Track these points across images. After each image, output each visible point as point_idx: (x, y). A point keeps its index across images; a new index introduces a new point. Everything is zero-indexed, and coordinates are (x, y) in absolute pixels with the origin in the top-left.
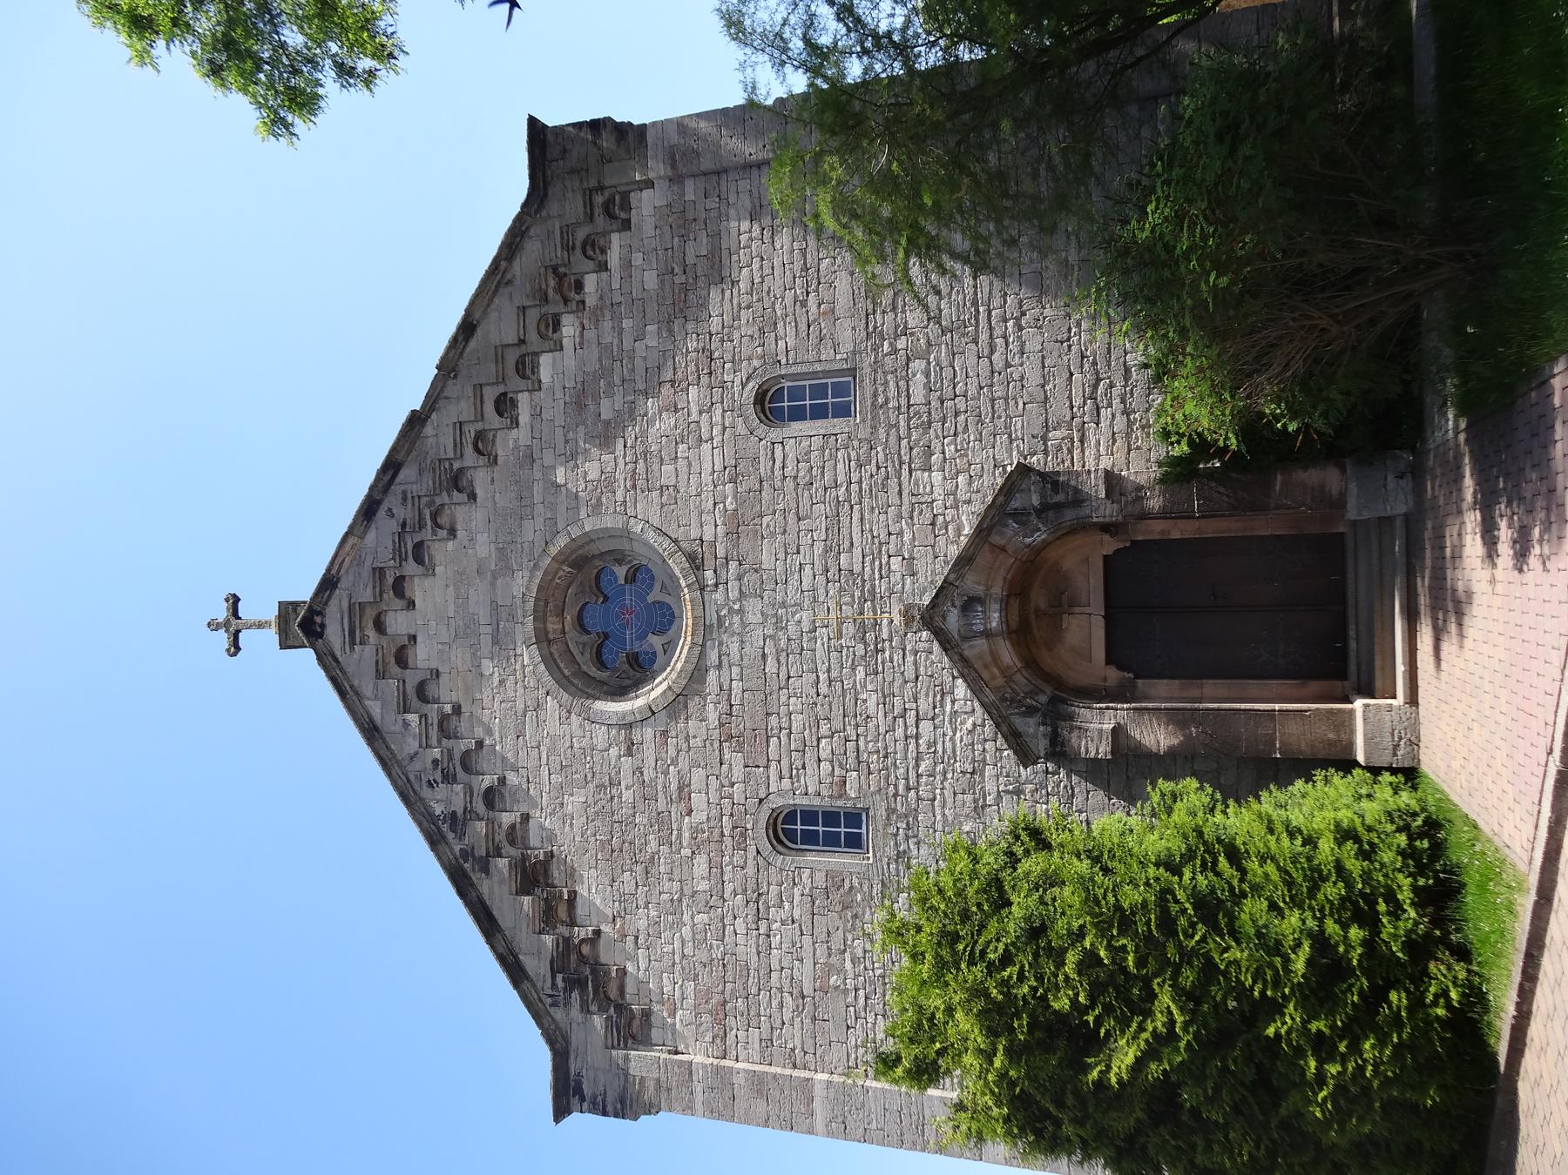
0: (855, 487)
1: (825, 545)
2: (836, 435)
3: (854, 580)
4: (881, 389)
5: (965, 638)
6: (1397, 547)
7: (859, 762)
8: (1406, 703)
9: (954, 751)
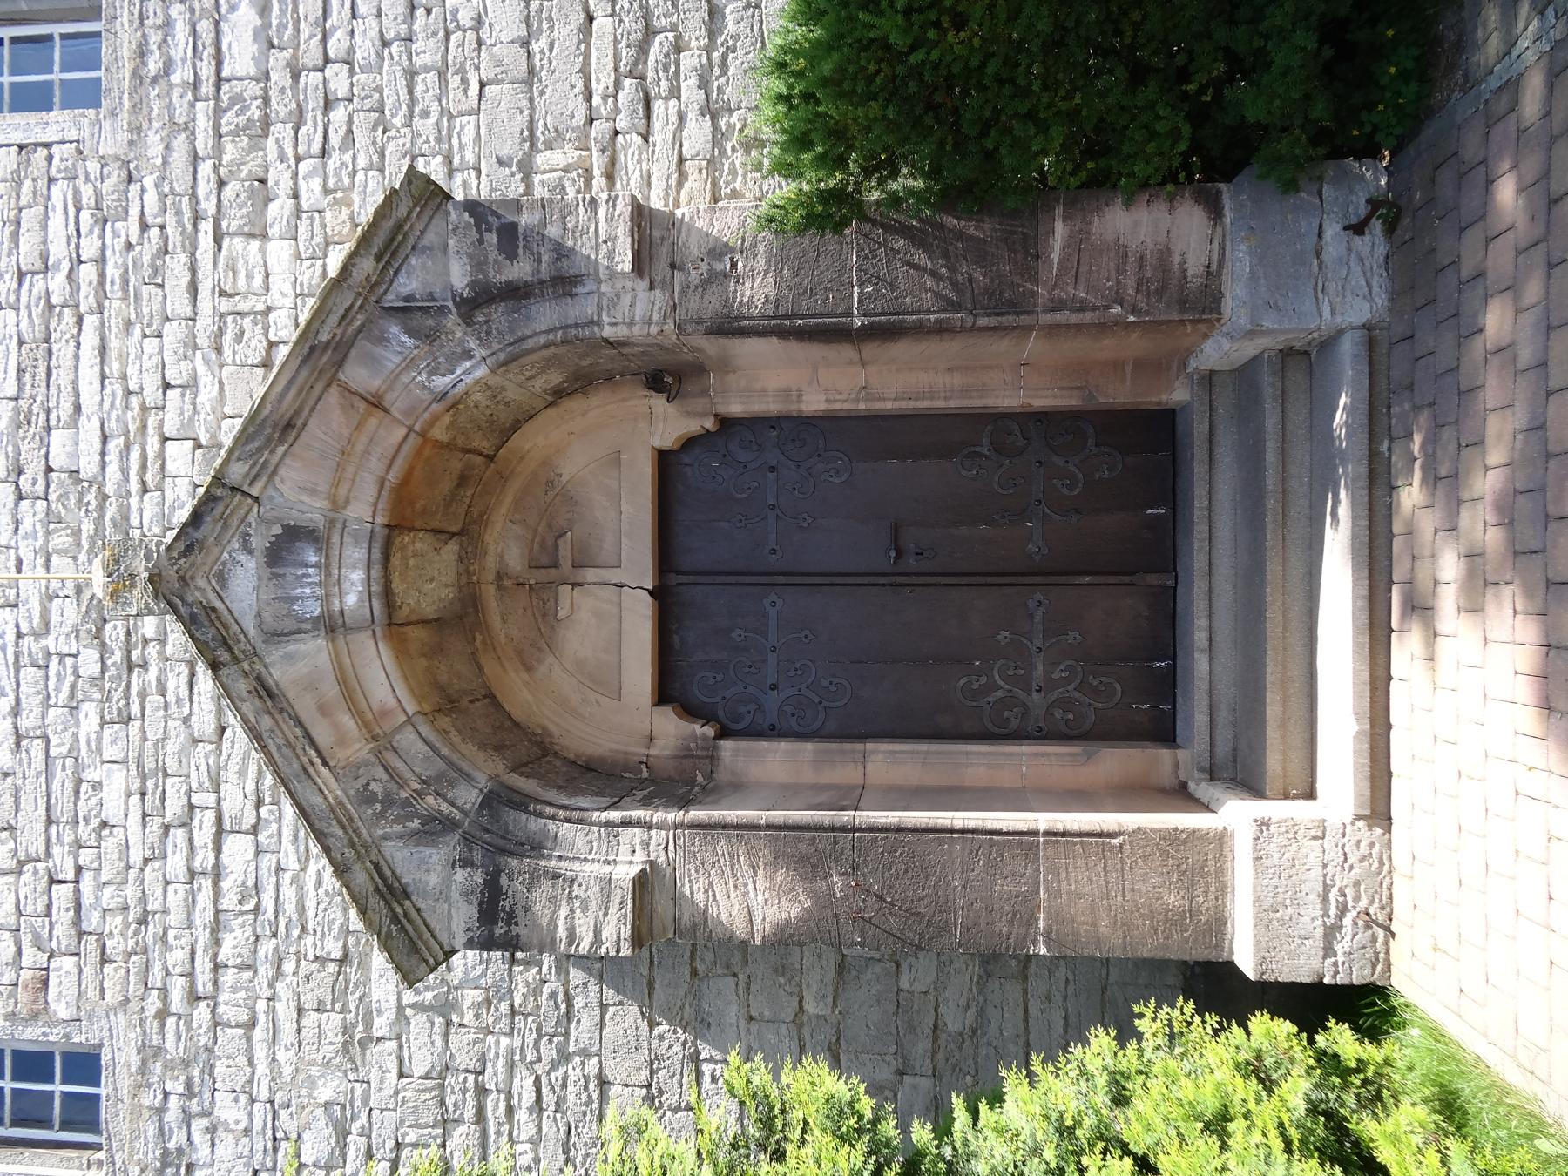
0: (87, 272)
1: (17, 410)
2: (47, 145)
3: (81, 494)
4: (154, 38)
5: (274, 636)
6: (1339, 419)
7: (81, 934)
8: (1359, 818)
9: (301, 909)
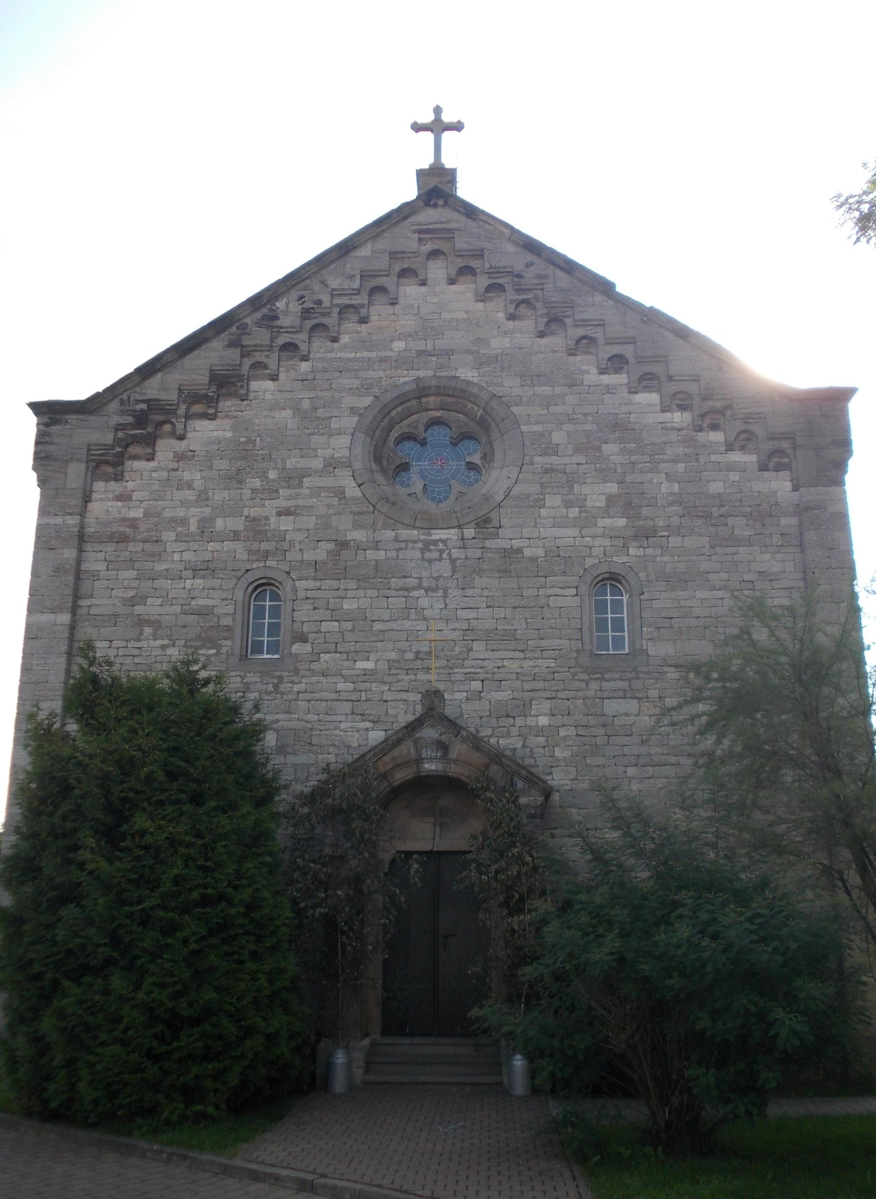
5: (416, 743)
